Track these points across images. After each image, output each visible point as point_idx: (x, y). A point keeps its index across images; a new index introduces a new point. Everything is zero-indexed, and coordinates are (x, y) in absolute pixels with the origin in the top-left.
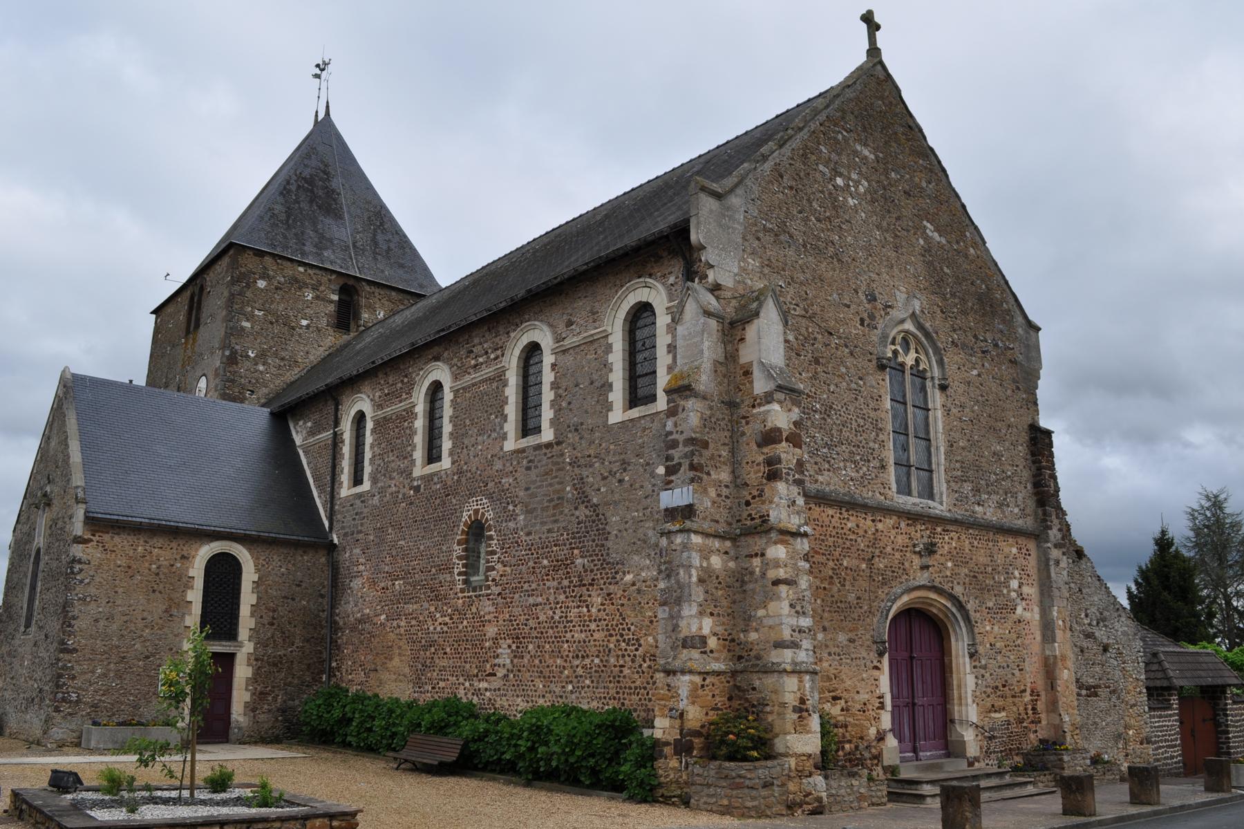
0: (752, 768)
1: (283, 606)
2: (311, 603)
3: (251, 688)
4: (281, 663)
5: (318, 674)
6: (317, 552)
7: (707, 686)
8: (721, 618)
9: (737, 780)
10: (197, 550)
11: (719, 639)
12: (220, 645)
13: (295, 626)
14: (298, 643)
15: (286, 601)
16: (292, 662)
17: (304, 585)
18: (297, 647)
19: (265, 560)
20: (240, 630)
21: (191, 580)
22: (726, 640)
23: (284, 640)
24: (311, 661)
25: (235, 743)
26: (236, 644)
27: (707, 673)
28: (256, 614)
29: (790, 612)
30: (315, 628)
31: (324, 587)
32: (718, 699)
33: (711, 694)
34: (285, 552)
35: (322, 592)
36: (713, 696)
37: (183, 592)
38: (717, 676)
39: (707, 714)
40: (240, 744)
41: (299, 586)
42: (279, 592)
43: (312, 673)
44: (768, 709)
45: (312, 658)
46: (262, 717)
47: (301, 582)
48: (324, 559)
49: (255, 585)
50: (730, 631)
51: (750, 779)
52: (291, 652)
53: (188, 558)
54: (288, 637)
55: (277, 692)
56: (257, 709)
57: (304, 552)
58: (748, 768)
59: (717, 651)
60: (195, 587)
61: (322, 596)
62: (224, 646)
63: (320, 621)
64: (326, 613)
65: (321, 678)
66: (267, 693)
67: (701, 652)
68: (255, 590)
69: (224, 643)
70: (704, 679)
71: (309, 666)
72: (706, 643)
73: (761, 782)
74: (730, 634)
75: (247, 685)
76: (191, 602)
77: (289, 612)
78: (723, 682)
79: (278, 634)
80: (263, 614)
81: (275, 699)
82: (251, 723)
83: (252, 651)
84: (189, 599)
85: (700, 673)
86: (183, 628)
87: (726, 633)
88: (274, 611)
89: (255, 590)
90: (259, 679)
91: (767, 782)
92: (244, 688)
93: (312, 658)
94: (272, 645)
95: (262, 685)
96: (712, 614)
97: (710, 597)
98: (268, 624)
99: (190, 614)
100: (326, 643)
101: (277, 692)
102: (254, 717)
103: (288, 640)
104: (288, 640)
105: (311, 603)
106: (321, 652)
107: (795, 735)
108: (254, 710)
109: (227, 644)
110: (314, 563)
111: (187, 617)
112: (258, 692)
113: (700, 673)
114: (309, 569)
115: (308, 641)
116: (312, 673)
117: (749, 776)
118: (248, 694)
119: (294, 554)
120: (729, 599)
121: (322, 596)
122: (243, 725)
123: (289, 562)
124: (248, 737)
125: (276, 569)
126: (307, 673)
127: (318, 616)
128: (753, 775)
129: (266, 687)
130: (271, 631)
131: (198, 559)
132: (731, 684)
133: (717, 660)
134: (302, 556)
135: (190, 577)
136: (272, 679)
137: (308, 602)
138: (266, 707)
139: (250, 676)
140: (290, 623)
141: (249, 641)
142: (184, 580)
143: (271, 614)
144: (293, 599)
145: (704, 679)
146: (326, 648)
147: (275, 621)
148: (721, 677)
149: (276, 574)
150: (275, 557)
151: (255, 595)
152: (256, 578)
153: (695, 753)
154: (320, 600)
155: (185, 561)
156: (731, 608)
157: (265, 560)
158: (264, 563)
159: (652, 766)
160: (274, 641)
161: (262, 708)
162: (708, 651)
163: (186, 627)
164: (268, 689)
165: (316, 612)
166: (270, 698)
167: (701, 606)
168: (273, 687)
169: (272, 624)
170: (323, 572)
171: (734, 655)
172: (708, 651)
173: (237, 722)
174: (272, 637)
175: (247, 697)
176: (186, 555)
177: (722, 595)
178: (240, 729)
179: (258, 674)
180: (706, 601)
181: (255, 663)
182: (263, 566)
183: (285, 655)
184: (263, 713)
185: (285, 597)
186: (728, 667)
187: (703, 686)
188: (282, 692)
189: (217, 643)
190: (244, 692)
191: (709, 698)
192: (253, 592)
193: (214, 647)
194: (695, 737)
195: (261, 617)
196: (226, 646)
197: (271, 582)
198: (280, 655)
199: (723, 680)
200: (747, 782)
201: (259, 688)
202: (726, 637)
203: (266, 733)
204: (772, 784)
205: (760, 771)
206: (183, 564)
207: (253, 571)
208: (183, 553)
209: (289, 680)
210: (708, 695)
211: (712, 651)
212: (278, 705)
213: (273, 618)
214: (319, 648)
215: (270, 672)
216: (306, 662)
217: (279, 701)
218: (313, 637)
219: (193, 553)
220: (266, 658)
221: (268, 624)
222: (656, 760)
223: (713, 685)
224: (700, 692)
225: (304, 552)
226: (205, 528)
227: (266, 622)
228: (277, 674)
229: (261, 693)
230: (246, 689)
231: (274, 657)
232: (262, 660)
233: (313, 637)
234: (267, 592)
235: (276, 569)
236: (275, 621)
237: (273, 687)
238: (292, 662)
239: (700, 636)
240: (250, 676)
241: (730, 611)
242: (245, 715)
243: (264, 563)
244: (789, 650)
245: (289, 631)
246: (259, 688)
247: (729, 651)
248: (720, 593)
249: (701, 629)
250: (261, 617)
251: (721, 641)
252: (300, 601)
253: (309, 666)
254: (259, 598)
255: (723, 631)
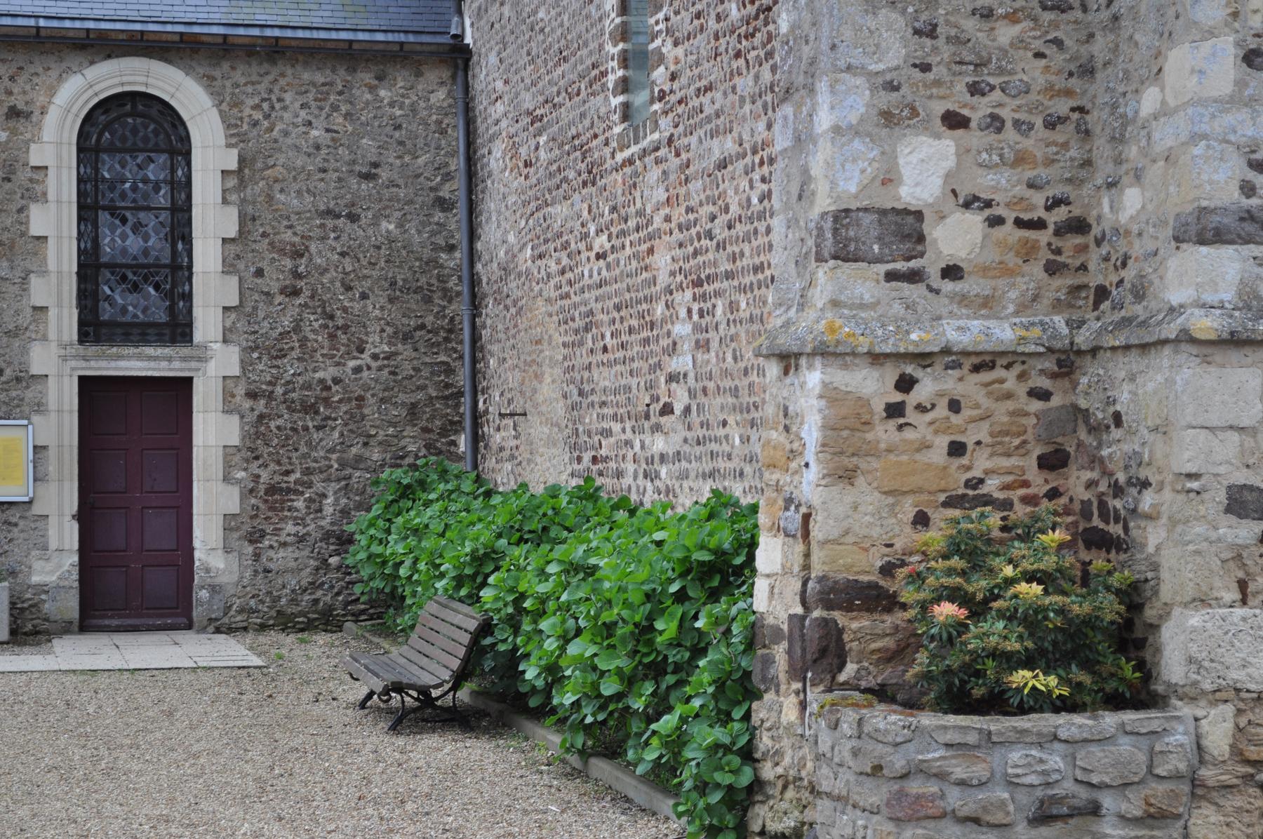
0: (972, 738)
1: (323, 239)
2: (412, 228)
3: (241, 475)
4: (326, 401)
5: (444, 432)
6: (419, 74)
7: (921, 408)
8: (1010, 133)
9: (915, 786)
10: (52, 91)
11: (995, 222)
12: (140, 357)
13: (364, 296)
14: (377, 343)
15: (330, 223)
16: (360, 399)
17: (384, 174)
18: (375, 357)
19: (257, 107)
20: (197, 312)
21: (38, 176)
22: (1039, 225)
23: (332, 337)
24: (420, 395)
25: (203, 630)
26: (185, 351)
27: (923, 358)
28: (241, 266)
29: (1241, 84)
30: (428, 300)
31: (448, 177)
32: (981, 463)
33: (942, 442)
34: (319, 78)
35: (445, 193)
36: (957, 449)
37: (20, 211)
38: (976, 369)
39: (921, 520)
40: (218, 631)
41: (367, 177)
42: (309, 199)
43: (426, 430)
44: (1148, 500)
45: (422, 388)
46: (282, 558)
47: (376, 165)
48: (441, 94)
49: (233, 182)
50: (1057, 191)
51: (962, 783)
52: (357, 370)
53: (28, 115)
54: (345, 328)
55: (319, 486)
56: (263, 534)
57: (380, 78)
58: (950, 737)
59: (984, 270)
60: (51, 195)
61: (444, 205)
62: (150, 358)
63: (442, 279)
64: (457, 254)
65: (454, 443)
66: (289, 490)
67: (891, 276)
68: (234, 197)
69: (150, 351)
70: (906, 384)
71: (413, 409)
72: (921, 239)
73: (1023, 797)
74: (1055, 203)
75: (228, 466)
76: (43, 239)
77: (343, 254)
78: (1009, 396)
79: (313, 321)
80: (264, 265)
81: (316, 506)
82: (248, 574)
83: (236, 371)
84: (35, 230)
85: (876, 358)
86: (29, 311)
87: (1039, 199)
88: (297, 254)
89: (234, 197)
90: (265, 451)
91: (1055, 800)
92: (221, 476)
93: (422, 388)
94: (295, 354)
95: (273, 466)
96: (954, 121)
97: (946, 52)
98: (282, 291)
99: (44, 273)
100: (461, 342)
101: (319, 486)
102: (257, 556)
103: (343, 338)
104: (343, 338)
105: (412, 228)
106: (449, 371)
107: (1239, 612)
108: (255, 537)
109: (159, 351)
110: (414, 110)
111: (34, 280)
112: (262, 487)
113: (876, 358)
114: (398, 127)
115: (407, 337)
116: (426, 430)
117: (959, 773)
118: (235, 492)
119: (347, 86)
120: (1058, 59)
121: (444, 205)
122: (223, 579)
123: (335, 108)
124: (241, 611)
125: (295, 132)
126: (409, 431)
127: (433, 262)
128: (979, 771)
129: (287, 473)
130: (293, 312)
131: (51, 121)
132: (1056, 401)
133: (987, 305)
134: (372, 89)
135: (36, 168)
136: (303, 449)
137: (400, 225)
138: (290, 528)
139: (235, 440)
140: (349, 288)
141: (225, 341)
142: (22, 176)
143: (288, 263)
144: (353, 218)
145: (906, 384)
146: (461, 357)
147: (301, 284)
148: (999, 373)
149: (297, 148)
150: (288, 97)
151: (233, 213)
152: (231, 160)
153: (850, 669)
154: (439, 216)
155: (21, 124)
156: (1068, 93)
157: (257, 107)
158: (258, 115)
159: (747, 717)
160: (303, 341)
161: (277, 531)
162: (934, 272)
163: (35, 308)
164: (292, 478)
165: (427, 253)
166: (300, 504)
167: (892, 87)
168: (308, 472)
169: (296, 293)
170: (443, 132)
171: (1080, 288)
172: (934, 272)
173: (208, 570)
174: (297, 329)
175: (231, 500)
176: (21, 106)
177: (1019, 43)
178: (214, 589)
179: (258, 435)
180: (925, 68)
181: (247, 404)
182: (255, 124)
183: (336, 381)
184: (284, 545)
185: (329, 213)
186: (1036, 332)
187: (894, 411)
188: (335, 486)
189: (132, 350)
190: (221, 486)
191: (938, 454)
192: (225, 201)
193: (122, 364)
194: (848, 608)
195: (259, 273)
196: (156, 358)
197: (279, 171)
198: (322, 381)
199: (1011, 384)
200: (955, 799)
201: (265, 476)
202: (1041, 213)
203: (294, 601)
204: (1094, 810)
205: (1015, 756)
206: (14, 132)
207: (222, 141)
208: (12, 101)
209: (354, 450)
210: (926, 446)
211: (952, 272)
212: (325, 523)
213: (297, 275)
214: (442, 358)
215: (294, 430)
216: (402, 397)
217: (328, 510)
218: (423, 327)
219: (41, 99)
220: (279, 390)
221: (282, 291)
222: (758, 696)
223: (955, 406)
224: (885, 432)
225: (380, 78)
226: (68, 24)
227: (275, 287)
228: (316, 436)
229: (272, 489)
230: (227, 479)
231: (307, 386)
232: (270, 396)
233: (423, 327)
234: (270, 198)
235: (295, 132)
236: (301, 284)
237: (308, 472)
238: (360, 399)
239: (883, 212)
240: (235, 440)
241: (1062, 107)
242: (227, 550)
243: (258, 115)
244: (1229, 250)
245: (345, 310)
246: (265, 476)
247: (1052, 269)
248: (1006, 33)
249: (889, 180)
250: (259, 273)
251: (1008, 231)
252: (375, 223)
253: (413, 409)
254: (245, 220)
255: (1020, 190)
